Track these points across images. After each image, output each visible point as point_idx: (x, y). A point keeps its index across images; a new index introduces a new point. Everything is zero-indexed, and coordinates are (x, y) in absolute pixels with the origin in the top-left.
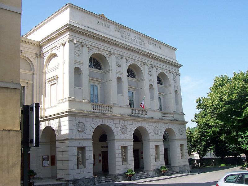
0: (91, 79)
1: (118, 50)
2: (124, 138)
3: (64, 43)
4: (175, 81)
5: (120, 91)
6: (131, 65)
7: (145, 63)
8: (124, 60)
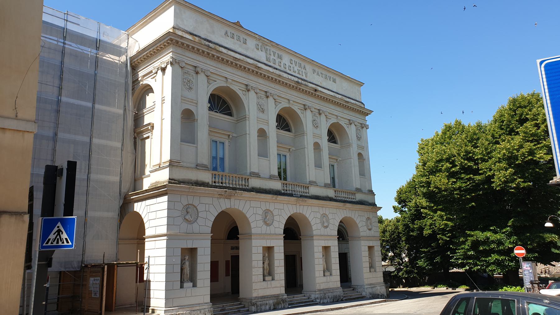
0: (212, 128)
1: (260, 83)
2: (268, 232)
3: (163, 66)
4: (359, 138)
5: (263, 153)
6: (284, 109)
7: (306, 107)
8: (271, 100)
